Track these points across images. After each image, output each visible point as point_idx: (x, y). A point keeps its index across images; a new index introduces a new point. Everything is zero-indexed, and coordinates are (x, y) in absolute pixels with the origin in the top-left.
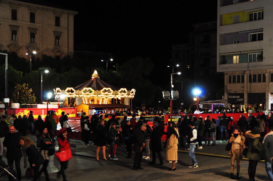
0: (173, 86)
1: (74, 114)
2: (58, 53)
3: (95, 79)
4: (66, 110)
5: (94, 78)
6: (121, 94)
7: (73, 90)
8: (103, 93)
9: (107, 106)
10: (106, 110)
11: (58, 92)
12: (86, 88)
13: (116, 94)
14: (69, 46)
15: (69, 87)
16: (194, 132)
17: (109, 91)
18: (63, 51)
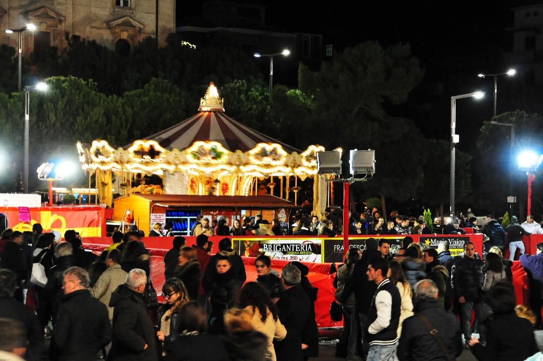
0: (456, 139)
1: (97, 226)
2: (125, 33)
3: (213, 114)
4: (70, 213)
5: (209, 109)
6: (310, 165)
7: (158, 147)
8: (257, 162)
9: (223, 202)
10: (211, 214)
11: (98, 153)
13: (296, 165)
14: (160, 11)
16: (381, 302)
17: (276, 154)
18: (142, 26)
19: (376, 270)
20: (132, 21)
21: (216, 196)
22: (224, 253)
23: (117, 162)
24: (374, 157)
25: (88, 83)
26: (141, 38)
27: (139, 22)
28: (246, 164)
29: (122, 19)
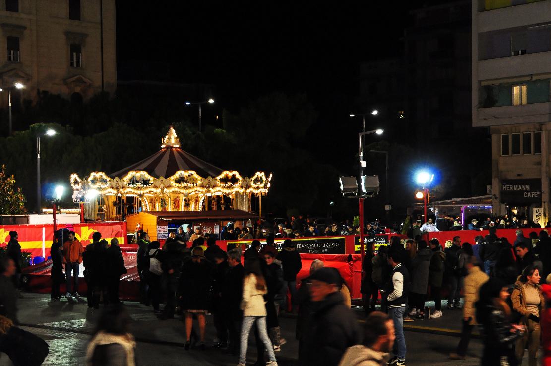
6: (256, 186)
7: (238, 176)
8: (177, 185)
12: (227, 172)
15: (94, 171)
18: (91, 82)
19: (523, 249)
20: (83, 78)
21: (191, 211)
22: (288, 249)
23: (112, 188)
24: (378, 181)
25: (66, 128)
26: (90, 94)
27: (89, 79)
28: (214, 187)
29: (76, 78)
